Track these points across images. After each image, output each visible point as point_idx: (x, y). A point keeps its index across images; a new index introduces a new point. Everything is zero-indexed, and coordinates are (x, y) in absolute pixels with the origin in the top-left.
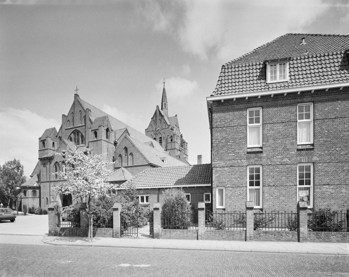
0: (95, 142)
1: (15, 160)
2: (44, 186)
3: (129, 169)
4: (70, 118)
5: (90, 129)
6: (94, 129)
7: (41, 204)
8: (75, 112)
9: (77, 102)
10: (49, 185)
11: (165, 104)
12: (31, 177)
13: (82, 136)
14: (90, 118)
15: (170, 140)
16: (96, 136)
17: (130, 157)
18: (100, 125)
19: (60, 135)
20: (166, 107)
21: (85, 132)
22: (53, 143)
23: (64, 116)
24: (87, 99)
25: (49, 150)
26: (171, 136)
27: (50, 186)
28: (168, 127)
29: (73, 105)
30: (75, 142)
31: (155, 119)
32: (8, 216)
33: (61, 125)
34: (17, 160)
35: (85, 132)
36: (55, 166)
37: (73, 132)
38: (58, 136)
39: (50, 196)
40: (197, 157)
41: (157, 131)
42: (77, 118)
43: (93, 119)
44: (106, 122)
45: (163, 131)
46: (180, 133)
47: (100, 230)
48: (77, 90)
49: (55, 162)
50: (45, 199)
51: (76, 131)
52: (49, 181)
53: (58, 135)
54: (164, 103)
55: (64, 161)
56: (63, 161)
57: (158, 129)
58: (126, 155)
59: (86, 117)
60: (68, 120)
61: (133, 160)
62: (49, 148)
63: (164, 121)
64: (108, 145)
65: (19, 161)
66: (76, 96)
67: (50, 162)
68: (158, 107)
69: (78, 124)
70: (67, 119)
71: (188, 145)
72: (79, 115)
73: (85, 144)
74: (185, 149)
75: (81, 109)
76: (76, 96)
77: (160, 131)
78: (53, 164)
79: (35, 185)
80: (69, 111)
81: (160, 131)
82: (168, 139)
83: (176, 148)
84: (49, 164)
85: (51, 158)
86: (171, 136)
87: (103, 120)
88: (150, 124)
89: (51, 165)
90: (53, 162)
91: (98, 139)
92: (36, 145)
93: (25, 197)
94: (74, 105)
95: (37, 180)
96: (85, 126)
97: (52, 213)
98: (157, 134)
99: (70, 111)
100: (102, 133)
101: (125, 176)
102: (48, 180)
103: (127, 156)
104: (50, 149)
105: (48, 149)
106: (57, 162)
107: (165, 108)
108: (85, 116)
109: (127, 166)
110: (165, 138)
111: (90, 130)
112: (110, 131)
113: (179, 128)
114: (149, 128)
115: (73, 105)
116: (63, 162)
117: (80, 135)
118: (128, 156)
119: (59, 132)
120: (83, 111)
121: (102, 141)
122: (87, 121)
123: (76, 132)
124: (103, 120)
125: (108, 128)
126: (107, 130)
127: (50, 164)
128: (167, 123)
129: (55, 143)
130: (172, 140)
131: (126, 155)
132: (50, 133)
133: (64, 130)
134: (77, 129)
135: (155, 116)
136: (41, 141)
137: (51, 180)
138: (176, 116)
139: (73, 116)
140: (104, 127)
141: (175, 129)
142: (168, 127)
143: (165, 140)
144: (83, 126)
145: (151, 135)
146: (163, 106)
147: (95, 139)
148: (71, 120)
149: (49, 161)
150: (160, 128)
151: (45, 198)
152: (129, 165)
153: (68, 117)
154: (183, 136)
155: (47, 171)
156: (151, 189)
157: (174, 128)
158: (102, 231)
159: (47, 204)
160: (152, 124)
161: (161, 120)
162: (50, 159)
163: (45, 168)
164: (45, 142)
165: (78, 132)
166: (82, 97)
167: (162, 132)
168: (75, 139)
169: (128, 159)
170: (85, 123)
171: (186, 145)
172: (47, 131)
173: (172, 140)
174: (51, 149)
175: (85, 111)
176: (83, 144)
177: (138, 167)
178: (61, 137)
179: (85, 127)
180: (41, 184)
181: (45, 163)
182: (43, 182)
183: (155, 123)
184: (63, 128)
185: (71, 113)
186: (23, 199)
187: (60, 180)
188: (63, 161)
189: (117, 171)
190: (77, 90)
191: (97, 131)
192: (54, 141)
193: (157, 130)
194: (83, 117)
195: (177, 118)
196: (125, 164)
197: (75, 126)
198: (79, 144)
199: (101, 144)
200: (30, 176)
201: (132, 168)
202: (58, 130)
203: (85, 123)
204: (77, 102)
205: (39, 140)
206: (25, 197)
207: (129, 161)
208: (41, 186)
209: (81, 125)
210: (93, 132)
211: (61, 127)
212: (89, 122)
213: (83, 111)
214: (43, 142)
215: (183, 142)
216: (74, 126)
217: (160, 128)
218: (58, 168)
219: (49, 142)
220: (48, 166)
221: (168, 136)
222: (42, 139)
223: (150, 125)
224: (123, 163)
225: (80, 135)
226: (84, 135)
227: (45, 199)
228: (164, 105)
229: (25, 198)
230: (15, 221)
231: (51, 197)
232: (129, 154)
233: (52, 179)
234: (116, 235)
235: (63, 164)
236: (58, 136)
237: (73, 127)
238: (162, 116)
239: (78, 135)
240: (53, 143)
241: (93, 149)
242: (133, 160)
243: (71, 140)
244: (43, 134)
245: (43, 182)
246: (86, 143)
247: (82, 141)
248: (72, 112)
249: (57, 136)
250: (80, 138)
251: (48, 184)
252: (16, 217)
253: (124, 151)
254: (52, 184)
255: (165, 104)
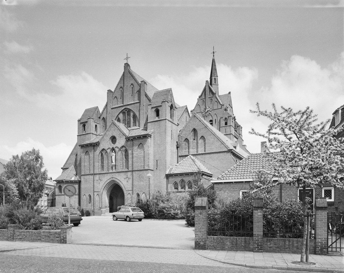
0: (156, 123)
1: (34, 150)
2: (86, 181)
3: (199, 157)
4: (118, 95)
5: (149, 106)
6: (155, 106)
7: (82, 201)
8: (125, 87)
9: (127, 73)
10: (93, 179)
11: (215, 78)
12: (63, 169)
13: (135, 116)
14: (146, 93)
15: (224, 123)
16: (158, 115)
17: (201, 141)
18: (164, 101)
19: (104, 115)
20: (216, 82)
21: (139, 111)
22: (96, 126)
23: (109, 91)
24: (140, 71)
25: (91, 134)
26: (226, 118)
27: (94, 180)
28: (222, 107)
29: (122, 77)
30: (125, 124)
31: (203, 97)
32: (74, 218)
33: (105, 103)
34: (36, 149)
35: (139, 111)
36: (100, 154)
37: (123, 112)
38: (102, 117)
39: (94, 194)
40: (260, 144)
41: (207, 112)
42: (128, 93)
43: (151, 95)
44: (170, 97)
45: (215, 112)
46: (233, 115)
47: (289, 242)
48: (127, 58)
49: (101, 149)
50: (87, 196)
51: (126, 111)
52: (93, 174)
53: (101, 116)
54: (213, 78)
55: (114, 147)
56: (113, 148)
57: (208, 110)
58: (194, 139)
59: (140, 93)
60: (116, 97)
61: (205, 146)
62: (91, 132)
63: (216, 100)
64: (172, 127)
65: (38, 151)
66: (127, 65)
67: (94, 149)
68: (207, 81)
69: (129, 100)
70: (114, 96)
71: (243, 129)
72: (131, 89)
73: (139, 126)
74: (240, 134)
75: (132, 81)
76: (127, 65)
77: (210, 112)
78: (98, 152)
79: (73, 179)
80: (116, 85)
81: (210, 112)
82: (221, 122)
83: (232, 133)
84: (92, 152)
85: (96, 144)
86: (226, 118)
87: (166, 94)
88: (197, 103)
89: (95, 153)
90: (98, 149)
91: (161, 119)
92: (75, 129)
93: (60, 194)
94: (124, 77)
95: (75, 173)
96: (140, 102)
97: (201, 214)
98: (207, 116)
99: (118, 85)
100: (165, 112)
101: (197, 165)
102: (92, 172)
103: (196, 141)
104: (93, 134)
105: (90, 133)
106: (103, 150)
107: (215, 84)
108: (139, 91)
109: (196, 153)
110: (216, 120)
111: (150, 107)
112: (174, 108)
113: (232, 108)
114: (195, 109)
115: (123, 78)
116: (113, 149)
117: (132, 114)
118: (197, 140)
119: (102, 113)
120: (135, 84)
121: (167, 120)
122: (142, 97)
123: (127, 112)
124: (166, 94)
125: (172, 105)
126: (172, 107)
127: (95, 151)
128: (219, 103)
129: (98, 126)
130: (226, 124)
131: (194, 139)
132: (93, 113)
133: (109, 108)
134: (128, 107)
135: (204, 94)
136: (81, 123)
137: (95, 173)
138: (230, 93)
139: (122, 91)
140: (168, 102)
141: (228, 109)
142: (222, 107)
143: (216, 123)
144: (136, 103)
145: (215, 114)
146: (213, 82)
147: (157, 119)
148: (119, 96)
149: (93, 148)
150: (211, 109)
151: (87, 195)
152: (200, 152)
153: (116, 92)
154: (236, 118)
155: (91, 162)
156: (235, 182)
157: (228, 108)
158: (293, 244)
159: (90, 203)
160: (201, 103)
161: (211, 99)
162: (94, 146)
163: (88, 156)
164: (86, 124)
165: (129, 111)
166: (133, 69)
167: (212, 113)
168: (124, 120)
169: (197, 144)
170: (139, 99)
171: (241, 129)
172: (87, 111)
173: (226, 124)
174: (93, 133)
175: (140, 85)
176: (136, 126)
177: (212, 155)
178: (105, 117)
179: (138, 104)
180: (82, 177)
181: (87, 151)
182: (84, 175)
183: (204, 102)
184: (108, 107)
185: (119, 87)
186: (58, 196)
187: (108, 172)
188: (113, 148)
189: (184, 160)
190: (127, 58)
191: (159, 108)
192: (96, 124)
193: (206, 111)
194: (135, 92)
195: (230, 97)
196: (193, 151)
197: (125, 104)
198: (130, 127)
199: (166, 125)
200: (62, 168)
201: (204, 156)
202: (101, 110)
203: (139, 99)
204: (127, 73)
205: (78, 123)
206: (60, 194)
207: (199, 146)
208: (82, 180)
209: (133, 102)
210: (154, 109)
211: (106, 105)
212: (145, 98)
213: (135, 84)
214: (83, 124)
215: (237, 126)
216: (123, 104)
217: (211, 109)
218: (105, 156)
219: (92, 124)
220: (91, 155)
221: (221, 118)
222: (82, 121)
223: (198, 105)
224: (191, 150)
225: (132, 114)
226: (137, 114)
227: (87, 196)
228: (213, 80)
229: (60, 195)
230: (79, 225)
231: (96, 194)
232: (199, 138)
233: (97, 171)
234: (323, 250)
235: (112, 152)
236: (102, 117)
237: (122, 105)
238: (213, 94)
239: (129, 115)
240: (96, 126)
241: (154, 131)
242: (205, 146)
243: (119, 120)
244: (83, 115)
245: (84, 175)
246: (141, 125)
247: (135, 122)
248: (121, 87)
249: (99, 118)
250: (132, 119)
251: (91, 177)
252: (82, 219)
253: (192, 134)
254: (97, 177)
255: (215, 78)
